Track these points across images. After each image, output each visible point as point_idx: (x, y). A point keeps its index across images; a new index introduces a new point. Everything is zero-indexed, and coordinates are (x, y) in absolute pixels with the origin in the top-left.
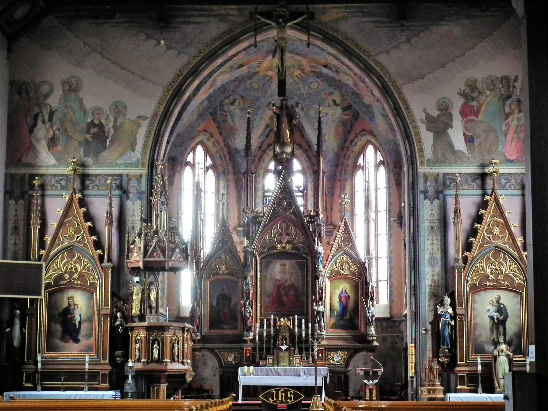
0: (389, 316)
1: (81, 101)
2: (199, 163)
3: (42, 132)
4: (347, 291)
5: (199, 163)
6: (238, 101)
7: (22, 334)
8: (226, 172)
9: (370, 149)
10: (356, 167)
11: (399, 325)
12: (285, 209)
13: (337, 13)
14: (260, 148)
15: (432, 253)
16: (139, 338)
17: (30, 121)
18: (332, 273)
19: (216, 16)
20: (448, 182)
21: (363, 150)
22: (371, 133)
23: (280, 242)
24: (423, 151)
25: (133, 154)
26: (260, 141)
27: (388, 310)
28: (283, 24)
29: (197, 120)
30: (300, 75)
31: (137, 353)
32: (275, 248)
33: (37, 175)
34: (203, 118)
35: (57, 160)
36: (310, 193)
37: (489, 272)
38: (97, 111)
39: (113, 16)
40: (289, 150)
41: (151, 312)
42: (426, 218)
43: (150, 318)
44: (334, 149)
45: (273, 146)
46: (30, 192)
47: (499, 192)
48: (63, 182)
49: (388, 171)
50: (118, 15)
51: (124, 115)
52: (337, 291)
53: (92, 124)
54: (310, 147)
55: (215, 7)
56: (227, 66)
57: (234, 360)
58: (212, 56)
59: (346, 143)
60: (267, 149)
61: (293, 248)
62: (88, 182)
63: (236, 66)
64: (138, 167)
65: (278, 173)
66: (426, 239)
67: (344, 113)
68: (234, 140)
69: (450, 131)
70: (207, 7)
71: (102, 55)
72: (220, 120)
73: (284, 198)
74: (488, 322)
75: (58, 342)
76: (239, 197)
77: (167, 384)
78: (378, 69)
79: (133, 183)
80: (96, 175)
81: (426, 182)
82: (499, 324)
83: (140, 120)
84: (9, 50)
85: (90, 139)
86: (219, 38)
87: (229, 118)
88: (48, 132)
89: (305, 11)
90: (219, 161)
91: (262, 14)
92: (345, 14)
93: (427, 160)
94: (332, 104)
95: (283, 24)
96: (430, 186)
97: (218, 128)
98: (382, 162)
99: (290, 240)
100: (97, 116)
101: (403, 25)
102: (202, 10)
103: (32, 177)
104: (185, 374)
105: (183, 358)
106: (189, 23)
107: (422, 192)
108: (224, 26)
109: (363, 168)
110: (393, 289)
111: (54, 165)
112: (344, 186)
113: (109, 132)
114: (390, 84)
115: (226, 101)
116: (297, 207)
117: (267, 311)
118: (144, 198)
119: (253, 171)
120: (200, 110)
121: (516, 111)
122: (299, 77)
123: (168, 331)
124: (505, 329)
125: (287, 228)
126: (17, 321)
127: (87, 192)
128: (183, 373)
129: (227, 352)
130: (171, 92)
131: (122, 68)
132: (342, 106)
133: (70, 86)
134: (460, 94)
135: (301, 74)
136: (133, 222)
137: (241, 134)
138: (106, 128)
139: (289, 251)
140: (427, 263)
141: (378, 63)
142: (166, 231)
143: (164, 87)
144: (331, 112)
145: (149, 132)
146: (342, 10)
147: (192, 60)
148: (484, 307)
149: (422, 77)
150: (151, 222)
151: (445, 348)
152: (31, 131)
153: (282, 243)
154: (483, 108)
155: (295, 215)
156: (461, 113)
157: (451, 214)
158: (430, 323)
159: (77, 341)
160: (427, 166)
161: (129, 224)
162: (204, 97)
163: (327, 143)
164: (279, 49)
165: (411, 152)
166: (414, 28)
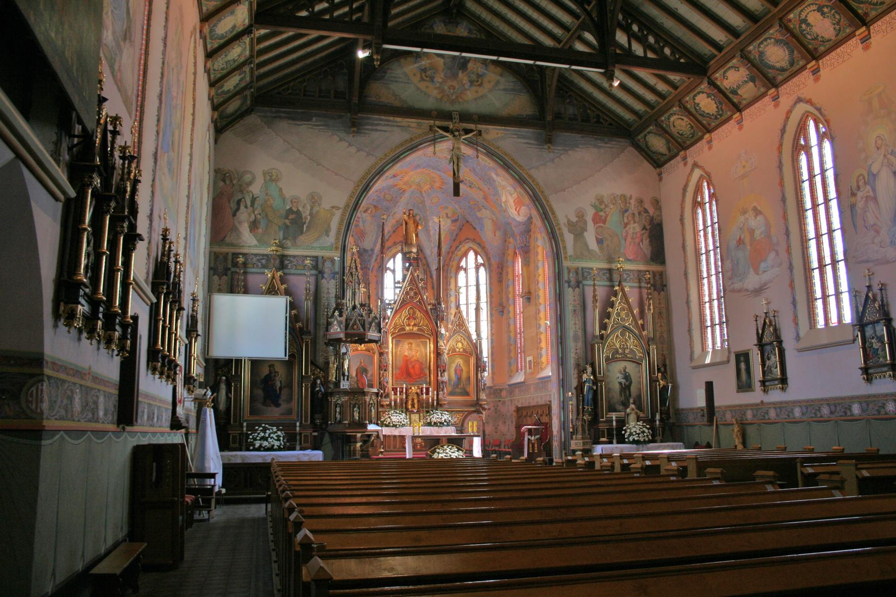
1: (281, 190)
3: (244, 215)
7: (228, 399)
9: (471, 254)
10: (459, 268)
12: (412, 298)
15: (576, 331)
16: (339, 402)
17: (233, 205)
18: (449, 350)
20: (586, 274)
21: (465, 254)
23: (409, 325)
31: (338, 416)
32: (404, 329)
35: (259, 241)
37: (618, 346)
38: (295, 200)
39: (310, 120)
46: (233, 269)
50: (314, 119)
51: (319, 205)
53: (290, 211)
55: (399, 119)
58: (396, 159)
61: (418, 330)
62: (287, 262)
69: (585, 234)
70: (391, 118)
71: (300, 153)
73: (411, 289)
75: (259, 406)
79: (328, 264)
80: (294, 257)
82: (625, 388)
87: (361, 224)
88: (250, 216)
91: (439, 127)
98: (483, 265)
100: (295, 204)
106: (377, 130)
107: (566, 282)
108: (407, 136)
111: (256, 246)
113: (306, 218)
125: (414, 313)
126: (223, 387)
127: (286, 271)
136: (328, 299)
138: (304, 215)
141: (530, 176)
145: (342, 221)
148: (615, 374)
151: (588, 408)
152: (234, 215)
161: (324, 301)
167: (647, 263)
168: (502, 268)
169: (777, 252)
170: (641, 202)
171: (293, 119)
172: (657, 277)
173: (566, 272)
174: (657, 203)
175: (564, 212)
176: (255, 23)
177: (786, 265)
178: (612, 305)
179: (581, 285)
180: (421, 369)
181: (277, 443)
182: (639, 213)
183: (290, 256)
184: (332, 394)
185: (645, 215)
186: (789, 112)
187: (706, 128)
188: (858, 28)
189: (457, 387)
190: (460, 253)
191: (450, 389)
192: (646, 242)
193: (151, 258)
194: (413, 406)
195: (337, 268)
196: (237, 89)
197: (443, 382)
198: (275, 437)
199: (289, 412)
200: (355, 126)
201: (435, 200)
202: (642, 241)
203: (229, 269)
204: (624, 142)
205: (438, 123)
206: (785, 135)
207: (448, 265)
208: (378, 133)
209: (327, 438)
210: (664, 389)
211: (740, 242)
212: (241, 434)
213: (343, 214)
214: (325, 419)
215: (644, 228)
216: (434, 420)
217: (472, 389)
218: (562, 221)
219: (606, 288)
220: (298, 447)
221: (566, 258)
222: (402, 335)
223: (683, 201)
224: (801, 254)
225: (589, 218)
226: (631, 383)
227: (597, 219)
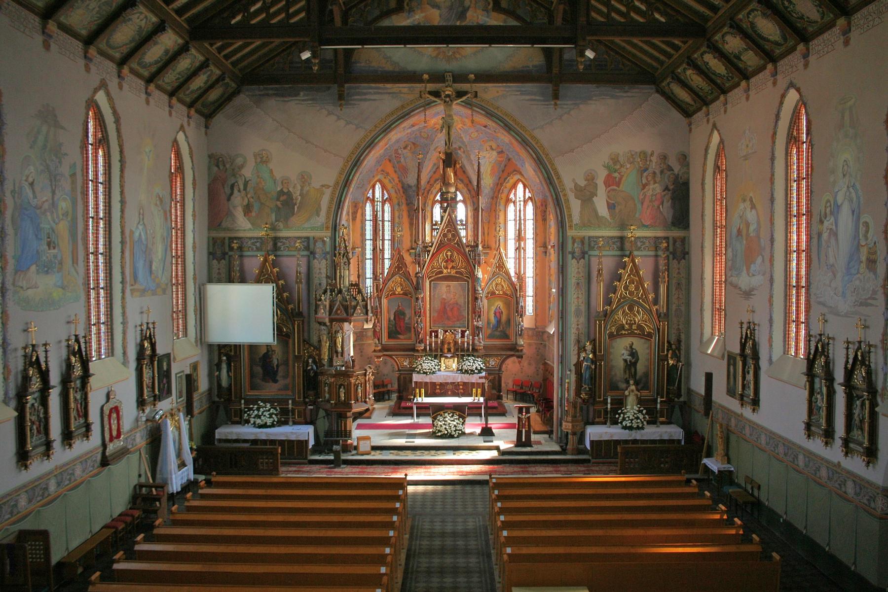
1: (271, 171)
3: (238, 200)
9: (520, 187)
10: (508, 201)
17: (227, 190)
19: (389, 93)
21: (514, 186)
22: (521, 173)
23: (446, 268)
27: (534, 322)
31: (327, 396)
32: (441, 272)
33: (236, 238)
35: (253, 224)
36: (470, 226)
37: (624, 322)
38: (285, 181)
39: (297, 95)
46: (231, 253)
47: (636, 253)
48: (258, 244)
49: (536, 208)
50: (302, 93)
53: (281, 193)
55: (388, 86)
61: (456, 273)
62: (279, 244)
69: (595, 199)
70: (381, 85)
74: (622, 364)
75: (258, 381)
76: (411, 224)
79: (319, 245)
80: (287, 238)
82: (631, 365)
84: (207, 127)
85: (280, 205)
87: (402, 160)
89: (469, 90)
91: (430, 93)
101: (556, 104)
103: (231, 239)
106: (365, 100)
107: (570, 253)
108: (397, 103)
109: (514, 203)
111: (250, 229)
113: (297, 199)
114: (544, 157)
116: (460, 238)
121: (652, 182)
124: (636, 370)
126: (224, 366)
127: (279, 253)
131: (307, 142)
133: (262, 158)
134: (604, 166)
136: (319, 279)
141: (533, 137)
144: (488, 155)
145: (332, 199)
148: (620, 350)
149: (572, 151)
152: (229, 199)
154: (624, 179)
156: (605, 183)
157: (594, 274)
159: (275, 381)
161: (316, 281)
164: (448, 126)
165: (562, 218)
167: (666, 227)
168: (546, 206)
169: (763, 257)
170: (664, 158)
171: (283, 96)
172: (678, 244)
173: (570, 241)
174: (684, 159)
175: (570, 176)
176: (190, 38)
177: (768, 275)
178: (619, 278)
179: (586, 256)
181: (269, 422)
182: (662, 172)
183: (283, 238)
184: (322, 374)
185: (669, 173)
186: (783, 96)
187: (703, 100)
188: (837, 17)
190: (509, 185)
191: (489, 331)
192: (668, 204)
193: (12, 378)
194: (449, 350)
195: (328, 249)
196: (210, 83)
197: (478, 327)
198: (267, 413)
199: (286, 388)
202: (662, 203)
203: (227, 253)
204: (649, 89)
205: (431, 87)
206: (780, 123)
208: (367, 103)
209: (322, 413)
210: (675, 367)
211: (739, 231)
212: (241, 410)
213: (333, 193)
214: (317, 395)
215: (667, 189)
216: (465, 367)
218: (568, 184)
219: (617, 258)
220: (291, 423)
221: (571, 227)
223: (705, 164)
224: (783, 267)
225: (600, 182)
226: (638, 360)
227: (610, 182)
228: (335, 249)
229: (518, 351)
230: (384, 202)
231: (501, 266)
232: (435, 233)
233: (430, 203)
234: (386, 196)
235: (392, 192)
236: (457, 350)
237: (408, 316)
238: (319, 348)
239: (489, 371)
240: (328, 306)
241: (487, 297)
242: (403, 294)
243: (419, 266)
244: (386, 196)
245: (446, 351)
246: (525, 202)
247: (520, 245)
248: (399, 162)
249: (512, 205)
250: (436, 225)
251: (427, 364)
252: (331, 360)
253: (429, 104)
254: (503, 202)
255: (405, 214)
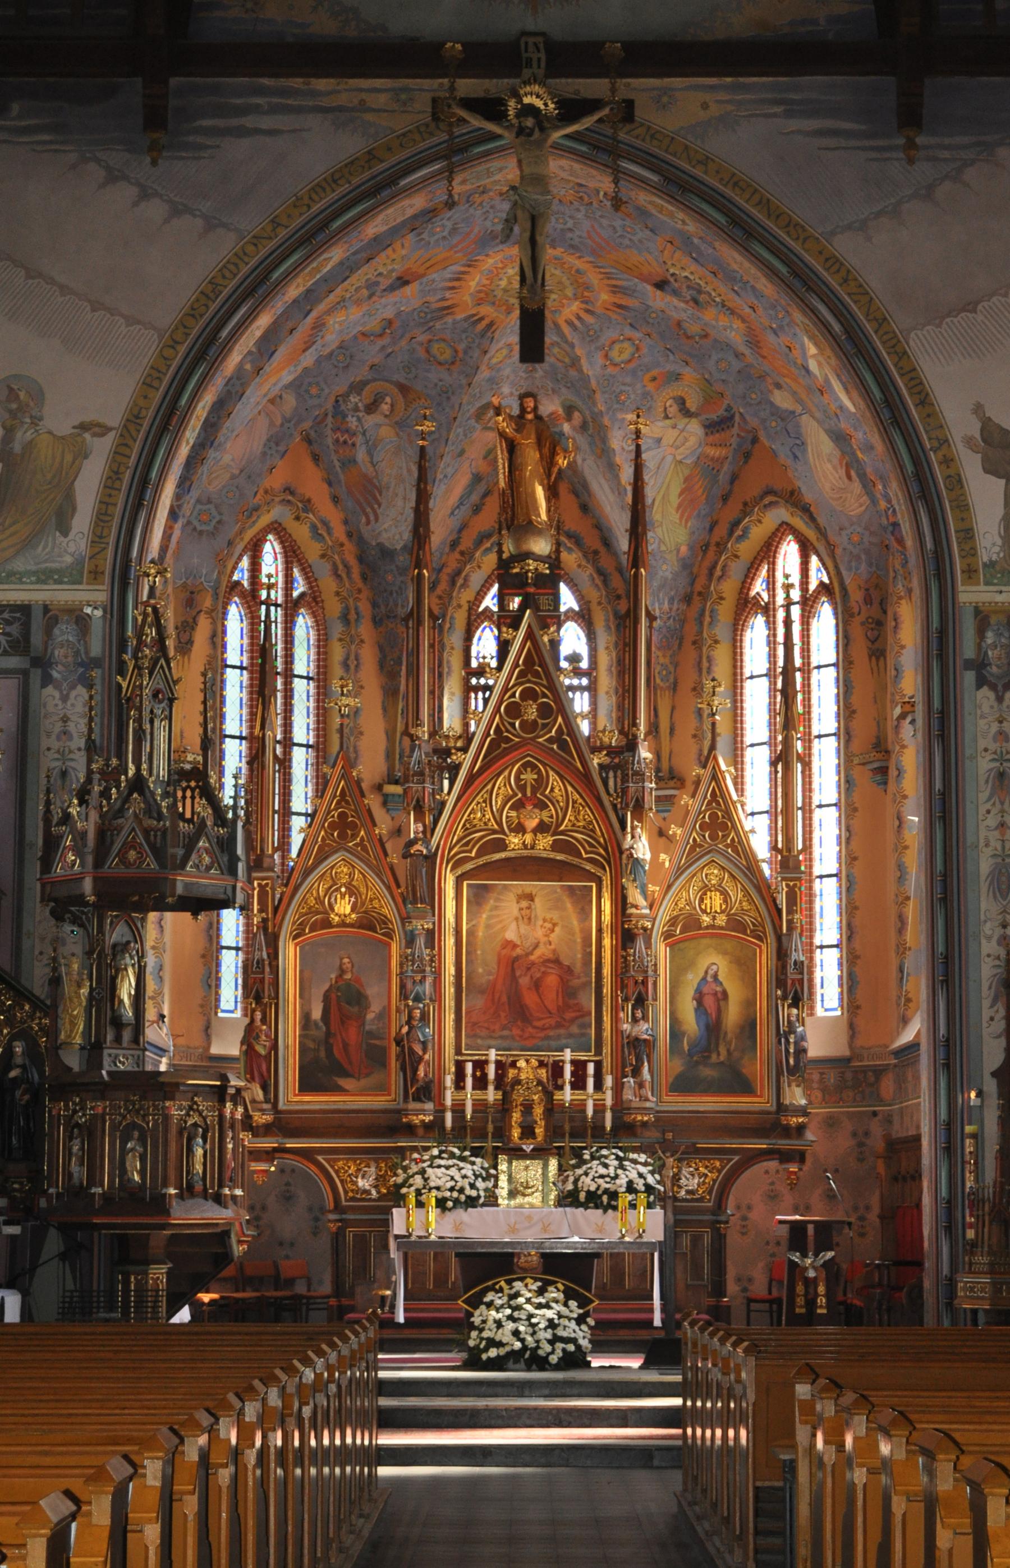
0: (847, 1053)
2: (270, 587)
4: (720, 978)
5: (270, 587)
6: (388, 399)
8: (352, 616)
9: (789, 554)
10: (746, 606)
11: (878, 1079)
12: (529, 727)
13: (705, 106)
14: (454, 544)
18: (673, 921)
21: (768, 552)
23: (520, 829)
24: (972, 537)
25: (62, 539)
26: (454, 523)
27: (844, 1039)
28: (537, 134)
29: (264, 454)
30: (579, 318)
34: (282, 448)
36: (606, 682)
40: (541, 546)
41: (118, 1039)
42: (982, 744)
43: (116, 1056)
44: (678, 551)
45: (494, 539)
50: (15, 108)
52: (690, 976)
54: (607, 542)
55: (322, 84)
56: (358, 279)
57: (376, 1187)
58: (313, 237)
59: (716, 530)
60: (476, 548)
61: (556, 846)
63: (385, 283)
64: (81, 583)
65: (507, 620)
66: (982, 810)
67: (711, 438)
68: (377, 520)
70: (297, 83)
72: (334, 458)
73: (528, 695)
76: (390, 693)
77: (576, 608)
78: (833, 282)
79: (65, 633)
81: (981, 633)
83: (87, 436)
86: (334, 179)
87: (361, 455)
90: (328, 585)
91: (471, 104)
92: (730, 107)
93: (985, 565)
94: (673, 410)
95: (537, 134)
96: (994, 646)
97: (330, 484)
99: (546, 819)
102: (283, 92)
104: (226, 1234)
105: (221, 1186)
106: (241, 132)
107: (969, 665)
108: (351, 145)
109: (768, 610)
110: (856, 969)
112: (710, 660)
114: (869, 328)
115: (354, 399)
117: (475, 1036)
118: (98, 681)
119: (436, 611)
120: (272, 424)
122: (577, 322)
123: (172, 1099)
125: (541, 783)
128: (219, 1230)
129: (376, 1161)
130: (182, 349)
132: (704, 417)
135: (582, 314)
136: (63, 755)
137: (400, 502)
139: (544, 854)
140: (984, 887)
141: (833, 262)
142: (168, 784)
143: (161, 337)
144: (670, 436)
146: (723, 96)
147: (250, 248)
149: (971, 307)
150: (121, 755)
153: (524, 832)
155: (563, 746)
158: (994, 1074)
160: (987, 584)
161: (50, 762)
162: (287, 377)
163: (659, 531)
164: (528, 223)
165: (937, 541)
166: (946, 154)
180: (568, 992)
189: (705, 1060)
190: (746, 548)
191: (677, 1066)
194: (528, 1132)
195: (96, 648)
200: (158, 127)
201: (621, 353)
205: (468, 86)
207: (704, 595)
213: (118, 453)
216: (588, 1183)
217: (758, 1067)
218: (960, 424)
221: (970, 573)
222: (494, 867)
228: (122, 647)
229: (787, 1132)
230: (291, 608)
231: (720, 822)
232: (477, 701)
233: (460, 618)
234: (300, 588)
235: (323, 571)
236: (554, 1132)
237: (375, 1007)
238: (50, 1007)
239: (682, 1216)
240: (91, 836)
241: (667, 935)
242: (360, 925)
243: (420, 818)
244: (300, 588)
245: (516, 1133)
246: (808, 604)
247: (787, 743)
248: (348, 463)
249: (759, 622)
250: (480, 672)
251: (446, 1172)
252: (94, 1049)
253: (464, 149)
254: (725, 611)
255: (368, 656)
